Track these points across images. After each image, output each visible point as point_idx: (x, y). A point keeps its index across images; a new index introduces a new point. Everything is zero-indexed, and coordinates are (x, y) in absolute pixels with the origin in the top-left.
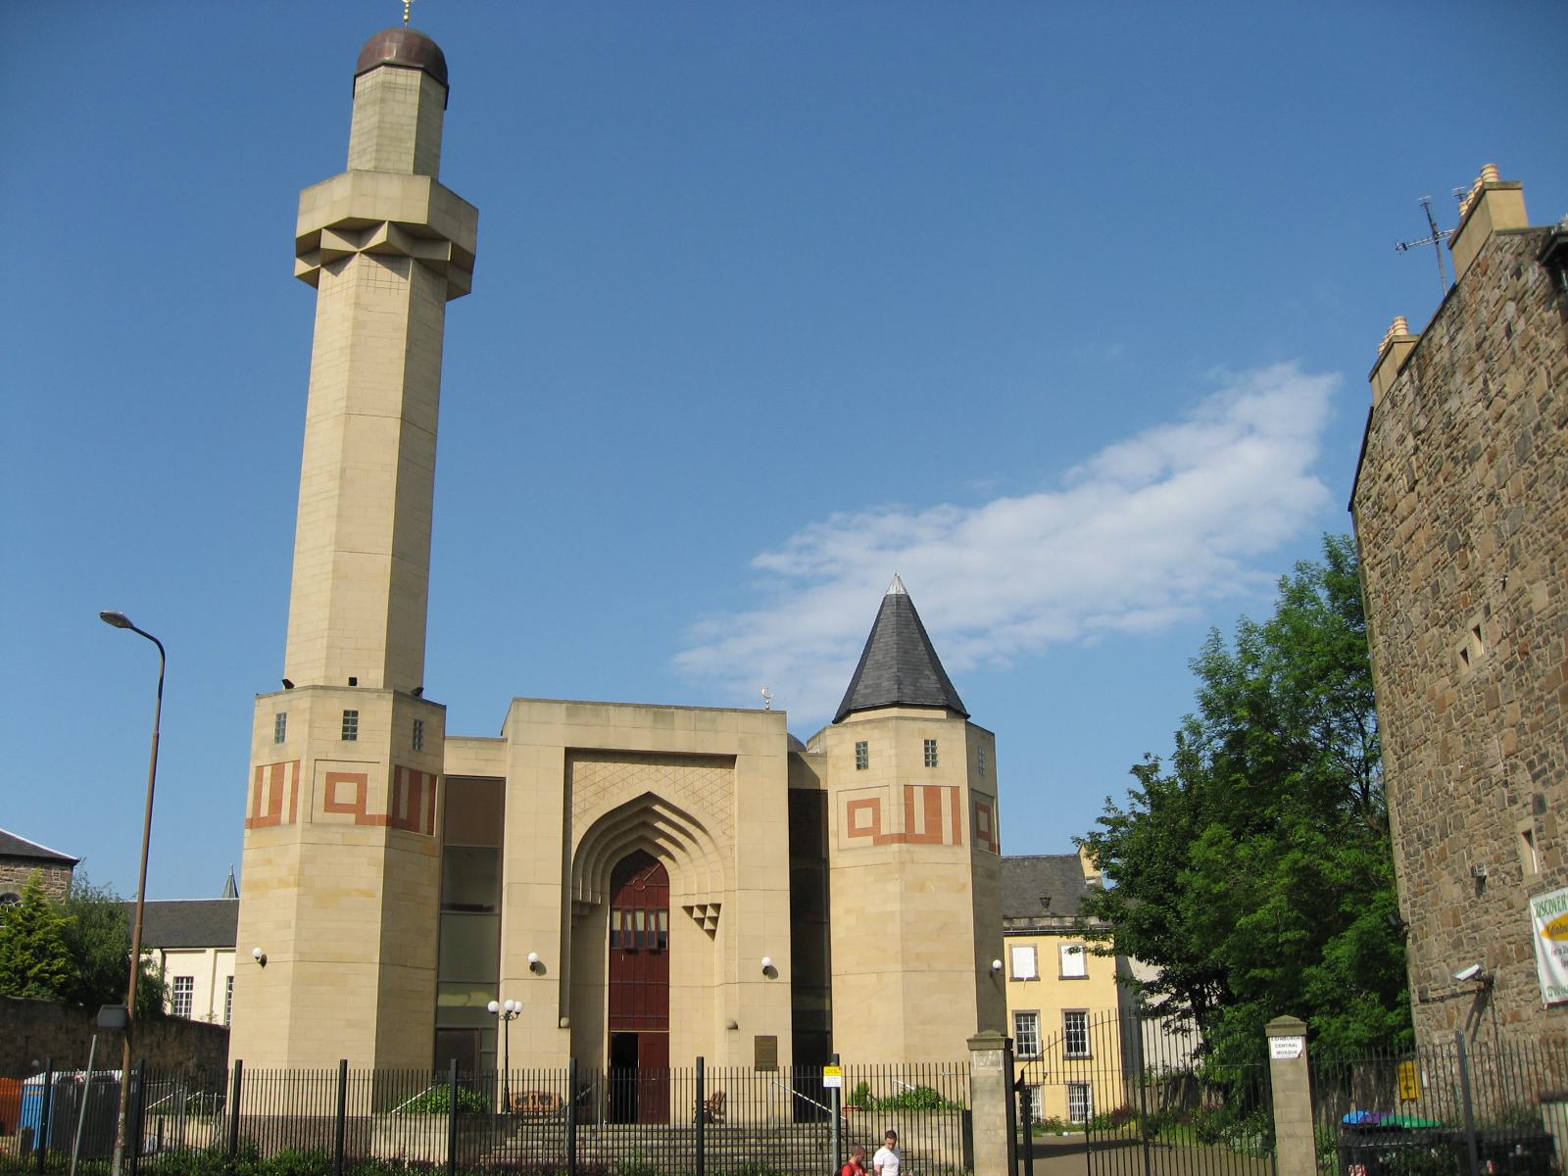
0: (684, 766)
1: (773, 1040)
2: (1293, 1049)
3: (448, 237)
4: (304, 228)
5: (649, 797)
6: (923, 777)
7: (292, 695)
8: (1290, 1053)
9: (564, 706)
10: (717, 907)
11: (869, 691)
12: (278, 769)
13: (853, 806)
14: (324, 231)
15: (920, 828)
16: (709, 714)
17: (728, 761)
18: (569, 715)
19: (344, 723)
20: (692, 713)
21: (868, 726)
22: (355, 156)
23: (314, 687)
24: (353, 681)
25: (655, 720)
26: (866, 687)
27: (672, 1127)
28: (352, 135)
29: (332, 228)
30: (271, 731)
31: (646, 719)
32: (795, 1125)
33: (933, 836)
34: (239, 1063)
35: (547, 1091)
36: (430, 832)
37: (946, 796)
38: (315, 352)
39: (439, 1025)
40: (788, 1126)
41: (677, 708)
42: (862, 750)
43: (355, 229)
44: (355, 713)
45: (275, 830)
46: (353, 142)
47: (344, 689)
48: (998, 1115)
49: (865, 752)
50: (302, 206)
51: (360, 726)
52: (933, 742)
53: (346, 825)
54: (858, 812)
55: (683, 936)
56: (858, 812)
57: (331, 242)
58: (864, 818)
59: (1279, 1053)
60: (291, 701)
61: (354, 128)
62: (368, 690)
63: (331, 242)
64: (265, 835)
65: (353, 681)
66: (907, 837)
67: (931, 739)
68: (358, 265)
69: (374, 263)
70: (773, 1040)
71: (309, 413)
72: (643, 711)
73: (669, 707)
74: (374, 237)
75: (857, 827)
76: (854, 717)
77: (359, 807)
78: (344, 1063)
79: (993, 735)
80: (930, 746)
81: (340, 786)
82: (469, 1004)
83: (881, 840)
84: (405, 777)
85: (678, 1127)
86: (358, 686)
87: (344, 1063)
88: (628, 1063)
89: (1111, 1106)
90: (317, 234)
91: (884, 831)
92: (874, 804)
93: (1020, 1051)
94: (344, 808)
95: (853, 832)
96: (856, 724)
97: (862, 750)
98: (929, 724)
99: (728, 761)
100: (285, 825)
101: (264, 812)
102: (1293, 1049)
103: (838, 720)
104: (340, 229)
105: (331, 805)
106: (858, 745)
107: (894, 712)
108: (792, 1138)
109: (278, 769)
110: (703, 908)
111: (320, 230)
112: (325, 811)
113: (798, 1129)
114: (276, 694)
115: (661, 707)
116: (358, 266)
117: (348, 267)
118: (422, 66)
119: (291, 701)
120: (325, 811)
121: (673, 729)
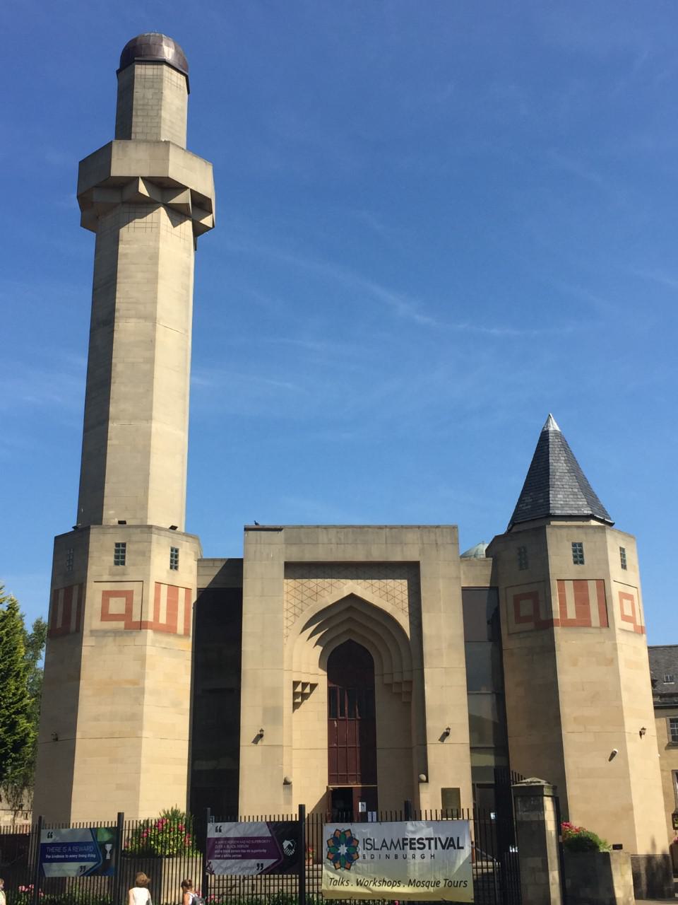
1: (457, 791)
3: (132, 174)
10: (295, 684)
29: (145, 179)
44: (124, 545)
49: (581, 551)
52: (580, 545)
70: (457, 791)
84: (164, 589)
94: (116, 617)
95: (105, 616)
101: (59, 625)
110: (399, 684)
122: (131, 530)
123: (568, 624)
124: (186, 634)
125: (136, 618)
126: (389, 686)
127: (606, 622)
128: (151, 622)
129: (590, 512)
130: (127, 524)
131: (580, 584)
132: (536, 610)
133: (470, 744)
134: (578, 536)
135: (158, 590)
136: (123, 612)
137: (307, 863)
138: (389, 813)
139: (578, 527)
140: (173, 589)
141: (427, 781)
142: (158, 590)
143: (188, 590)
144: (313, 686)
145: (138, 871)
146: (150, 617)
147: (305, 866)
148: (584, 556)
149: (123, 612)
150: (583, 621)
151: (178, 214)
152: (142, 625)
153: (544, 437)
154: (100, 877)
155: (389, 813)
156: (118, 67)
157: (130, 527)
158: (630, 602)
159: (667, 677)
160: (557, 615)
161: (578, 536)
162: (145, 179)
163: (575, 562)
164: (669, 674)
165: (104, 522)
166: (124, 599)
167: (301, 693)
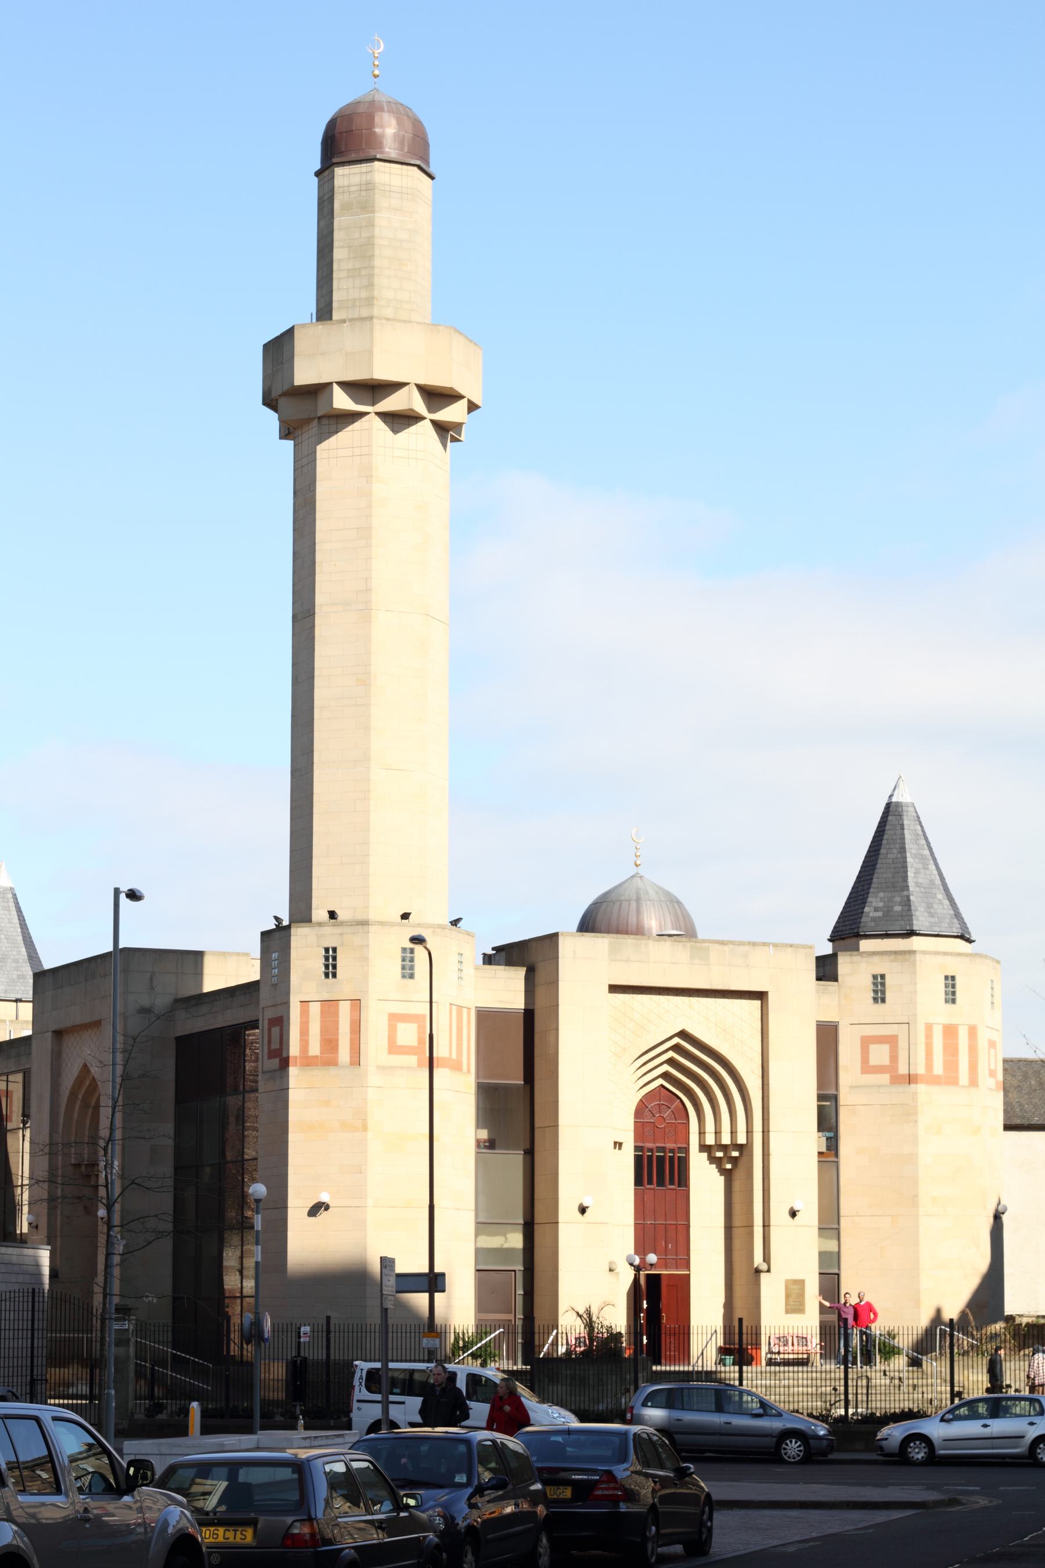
1: (801, 1283)
3: (463, 393)
11: (879, 914)
12: (950, 1032)
13: (866, 1042)
16: (742, 948)
19: (819, 1100)
20: (726, 948)
21: (885, 958)
24: (332, 915)
26: (876, 910)
29: (345, 385)
30: (318, 965)
34: (741, 1320)
36: (469, 1071)
37: (465, 1011)
44: (883, 976)
45: (332, 1071)
49: (883, 984)
56: (873, 1048)
57: (342, 401)
58: (879, 1055)
60: (342, 934)
63: (342, 401)
64: (317, 1074)
65: (332, 915)
67: (950, 974)
70: (801, 1283)
77: (891, 1068)
79: (265, 403)
81: (873, 1048)
82: (506, 1246)
89: (897, 1361)
92: (891, 1041)
94: (879, 1069)
95: (867, 1068)
98: (949, 958)
106: (875, 977)
109: (330, 1006)
117: (350, 428)
119: (342, 934)
123: (308, 1062)
125: (903, 1070)
127: (356, 1059)
128: (922, 1075)
130: (340, 918)
131: (330, 1006)
132: (894, 1058)
135: (929, 1036)
140: (460, 1008)
141: (769, 1271)
142: (929, 1036)
145: (405, 1380)
146: (920, 1069)
149: (886, 1061)
150: (328, 1057)
152: (911, 1079)
156: (318, 166)
157: (342, 924)
160: (294, 1050)
161: (880, 966)
162: (345, 385)
165: (313, 919)
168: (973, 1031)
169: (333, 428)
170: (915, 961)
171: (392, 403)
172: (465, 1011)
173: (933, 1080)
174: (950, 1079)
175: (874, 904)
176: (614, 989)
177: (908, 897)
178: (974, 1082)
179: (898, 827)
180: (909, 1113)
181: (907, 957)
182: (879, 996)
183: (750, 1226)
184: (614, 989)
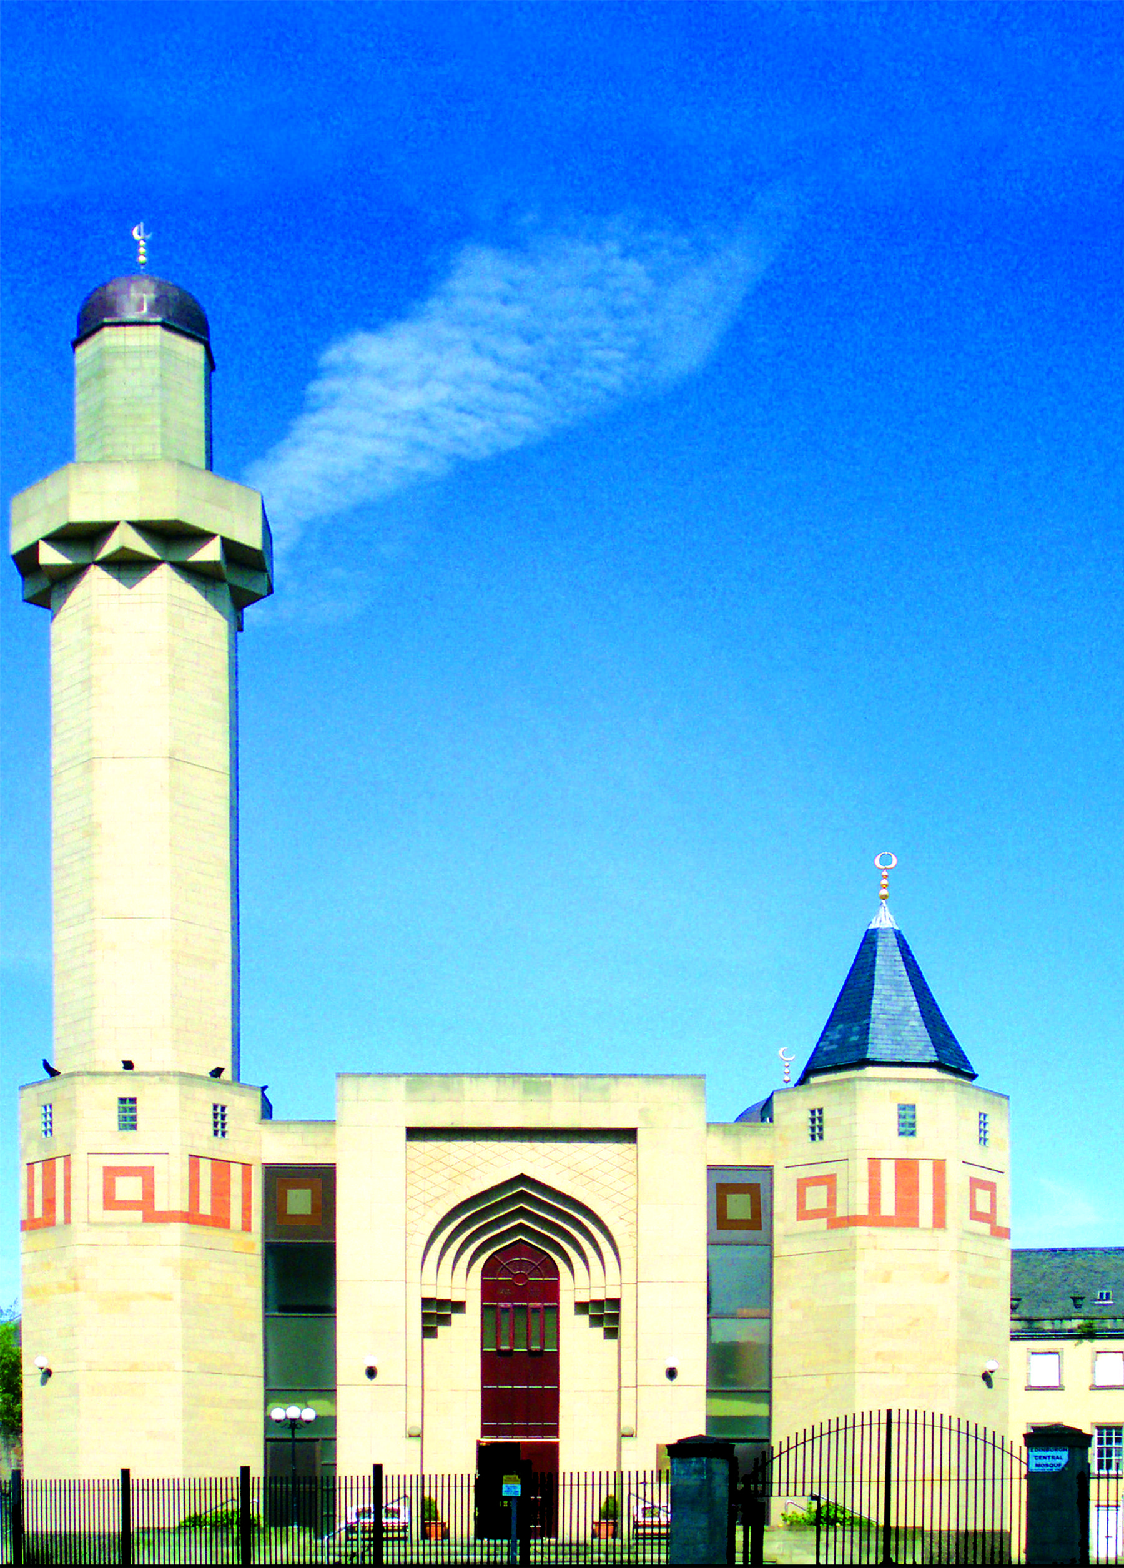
0: (450, 1141)
2: (1058, 1461)
4: (18, 543)
5: (522, 1179)
6: (207, 1145)
7: (58, 1082)
8: (1053, 1465)
9: (403, 1079)
11: (834, 1047)
12: (906, 1169)
14: (43, 546)
15: (205, 1208)
16: (600, 1082)
17: (628, 1135)
18: (410, 1089)
20: (576, 1081)
22: (83, 445)
23: (181, 1074)
25: (525, 1091)
27: (560, 1541)
28: (77, 420)
30: (38, 1125)
31: (512, 1090)
32: (479, 1542)
33: (219, 1220)
35: (865, 1514)
36: (247, 1227)
37: (236, 1171)
38: (55, 689)
39: (268, 1436)
40: (472, 1541)
41: (554, 1075)
42: (817, 1118)
43: (173, 536)
44: (133, 1100)
46: (79, 428)
47: (117, 1074)
48: (699, 1528)
50: (14, 519)
51: (140, 1114)
53: (131, 1224)
54: (810, 1191)
55: (576, 1338)
56: (810, 1191)
57: (49, 556)
58: (817, 1198)
59: (1037, 1465)
61: (79, 410)
62: (147, 1074)
66: (191, 1217)
68: (164, 578)
69: (176, 576)
71: (55, 762)
72: (509, 1081)
73: (546, 1075)
74: (106, 546)
75: (808, 1208)
76: (813, 1080)
77: (988, 1218)
78: (125, 1473)
80: (219, 1114)
83: (152, 1216)
84: (205, 1167)
85: (567, 1541)
86: (135, 1069)
87: (125, 1473)
88: (517, 1475)
90: (34, 549)
91: (160, 1205)
92: (829, 1181)
93: (1100, 1467)
94: (817, 1214)
95: (803, 1214)
96: (817, 1085)
97: (817, 1118)
99: (628, 1135)
100: (925, 1229)
101: (38, 1213)
102: (1058, 1461)
103: (802, 1081)
104: (65, 537)
105: (110, 1202)
107: (933, 1073)
108: (614, 1554)
109: (906, 1169)
111: (37, 543)
112: (105, 1209)
113: (549, 1545)
114: (40, 1083)
115: (532, 1075)
116: (164, 580)
118: (159, 319)
120: (105, 1209)
121: (550, 1101)
122: (139, 1078)
124: (247, 1227)
126: (581, 1307)
129: (936, 1059)
132: (832, 1200)
133: (708, 1384)
134: (910, 1093)
136: (139, 1197)
137: (385, 1549)
138: (465, 1478)
139: (826, 1083)
140: (221, 1166)
143: (247, 1167)
144: (459, 1307)
147: (529, 1554)
148: (138, 1118)
149: (139, 1197)
151: (128, 566)
153: (870, 940)
154: (979, 1562)
155: (465, 1478)
157: (244, 1086)
158: (988, 1193)
159: (1101, 1294)
161: (910, 1093)
163: (122, 1127)
164: (1103, 1288)
166: (139, 1179)
167: (436, 1314)
168: (939, 1167)
169: (198, 545)
170: (855, 1089)
171: (110, 547)
172: (236, 1171)
173: (874, 1219)
174: (906, 1216)
175: (831, 1038)
176: (414, 1133)
177: (868, 1024)
178: (939, 1222)
179: (871, 955)
180: (846, 1258)
181: (846, 1084)
182: (816, 1130)
183: (265, 1489)
184: (414, 1133)
